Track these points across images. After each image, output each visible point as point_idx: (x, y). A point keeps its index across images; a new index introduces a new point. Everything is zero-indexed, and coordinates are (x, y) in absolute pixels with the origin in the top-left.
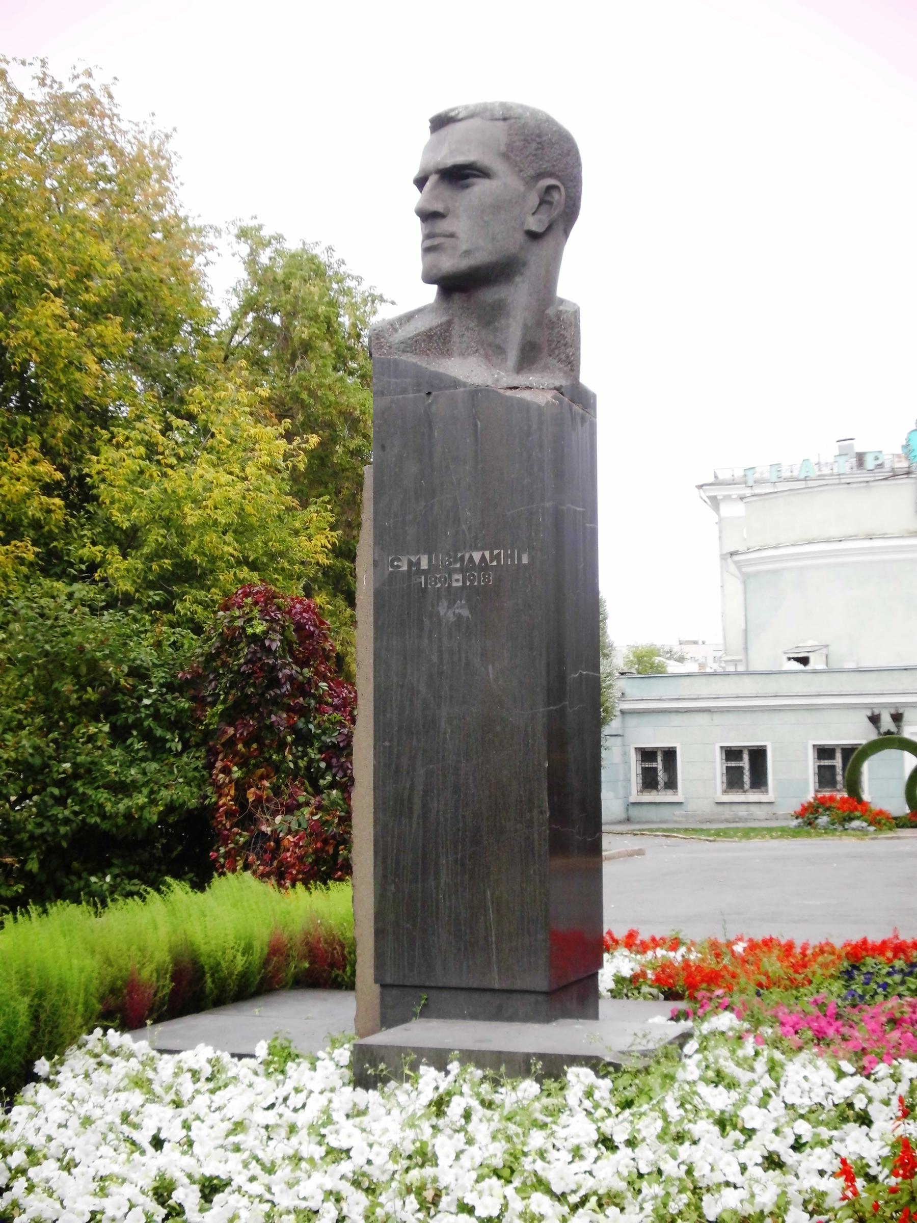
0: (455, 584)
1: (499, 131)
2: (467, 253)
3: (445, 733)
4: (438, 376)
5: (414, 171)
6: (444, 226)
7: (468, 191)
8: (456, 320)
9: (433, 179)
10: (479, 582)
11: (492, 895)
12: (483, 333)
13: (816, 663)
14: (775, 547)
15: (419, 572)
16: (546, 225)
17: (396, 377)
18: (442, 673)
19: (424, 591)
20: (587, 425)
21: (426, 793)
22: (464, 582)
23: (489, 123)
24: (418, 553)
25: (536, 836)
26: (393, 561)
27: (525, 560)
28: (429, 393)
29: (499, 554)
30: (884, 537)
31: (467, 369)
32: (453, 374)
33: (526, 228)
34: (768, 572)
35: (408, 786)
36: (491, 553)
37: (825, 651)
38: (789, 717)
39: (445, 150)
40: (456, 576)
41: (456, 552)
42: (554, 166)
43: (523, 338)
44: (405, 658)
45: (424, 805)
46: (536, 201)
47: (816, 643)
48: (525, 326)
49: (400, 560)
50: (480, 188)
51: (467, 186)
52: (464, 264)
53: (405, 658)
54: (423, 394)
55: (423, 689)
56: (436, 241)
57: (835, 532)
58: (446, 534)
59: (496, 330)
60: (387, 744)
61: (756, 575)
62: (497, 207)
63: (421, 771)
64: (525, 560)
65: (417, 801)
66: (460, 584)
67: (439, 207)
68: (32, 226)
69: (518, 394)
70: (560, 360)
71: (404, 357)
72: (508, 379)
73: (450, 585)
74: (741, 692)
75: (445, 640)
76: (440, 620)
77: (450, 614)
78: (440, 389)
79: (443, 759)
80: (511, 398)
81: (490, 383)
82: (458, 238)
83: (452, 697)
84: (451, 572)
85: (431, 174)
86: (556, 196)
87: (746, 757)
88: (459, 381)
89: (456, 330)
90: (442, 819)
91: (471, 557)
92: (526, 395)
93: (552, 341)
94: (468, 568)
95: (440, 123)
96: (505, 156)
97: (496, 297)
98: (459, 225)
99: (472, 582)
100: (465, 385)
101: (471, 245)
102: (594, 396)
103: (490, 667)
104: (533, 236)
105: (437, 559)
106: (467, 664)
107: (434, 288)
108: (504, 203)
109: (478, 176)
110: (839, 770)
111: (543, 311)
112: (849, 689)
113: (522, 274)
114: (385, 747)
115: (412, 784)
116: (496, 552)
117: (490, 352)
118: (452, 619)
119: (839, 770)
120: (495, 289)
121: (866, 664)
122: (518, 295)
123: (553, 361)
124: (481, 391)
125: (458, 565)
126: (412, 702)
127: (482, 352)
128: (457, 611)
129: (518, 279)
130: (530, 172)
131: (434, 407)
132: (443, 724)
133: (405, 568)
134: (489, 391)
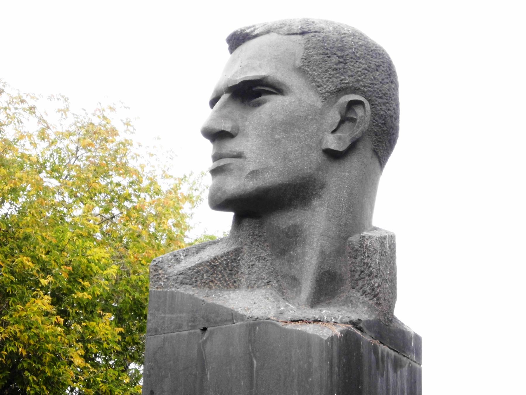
1: (297, 46)
2: (254, 173)
4: (216, 309)
5: (209, 95)
6: (231, 146)
9: (225, 97)
12: (277, 263)
16: (348, 143)
17: (172, 312)
20: (405, 371)
23: (285, 37)
28: (205, 329)
31: (249, 301)
32: (231, 307)
33: (324, 147)
39: (237, 67)
42: (358, 81)
43: (320, 266)
46: (338, 118)
48: (322, 252)
50: (273, 104)
51: (259, 104)
52: (251, 185)
54: (198, 331)
56: (222, 162)
62: (290, 124)
67: (227, 126)
68: (29, 230)
70: (364, 292)
71: (182, 290)
72: (293, 311)
78: (216, 323)
80: (290, 331)
81: (271, 316)
85: (222, 94)
86: (359, 112)
89: (245, 259)
92: (310, 329)
95: (237, 40)
96: (301, 71)
97: (291, 222)
98: (248, 144)
100: (242, 317)
101: (261, 162)
102: (418, 339)
104: (333, 155)
107: (229, 217)
108: (317, 133)
109: (271, 93)
111: (346, 239)
117: (285, 285)
122: (316, 222)
124: (259, 324)
127: (274, 284)
129: (315, 202)
130: (331, 87)
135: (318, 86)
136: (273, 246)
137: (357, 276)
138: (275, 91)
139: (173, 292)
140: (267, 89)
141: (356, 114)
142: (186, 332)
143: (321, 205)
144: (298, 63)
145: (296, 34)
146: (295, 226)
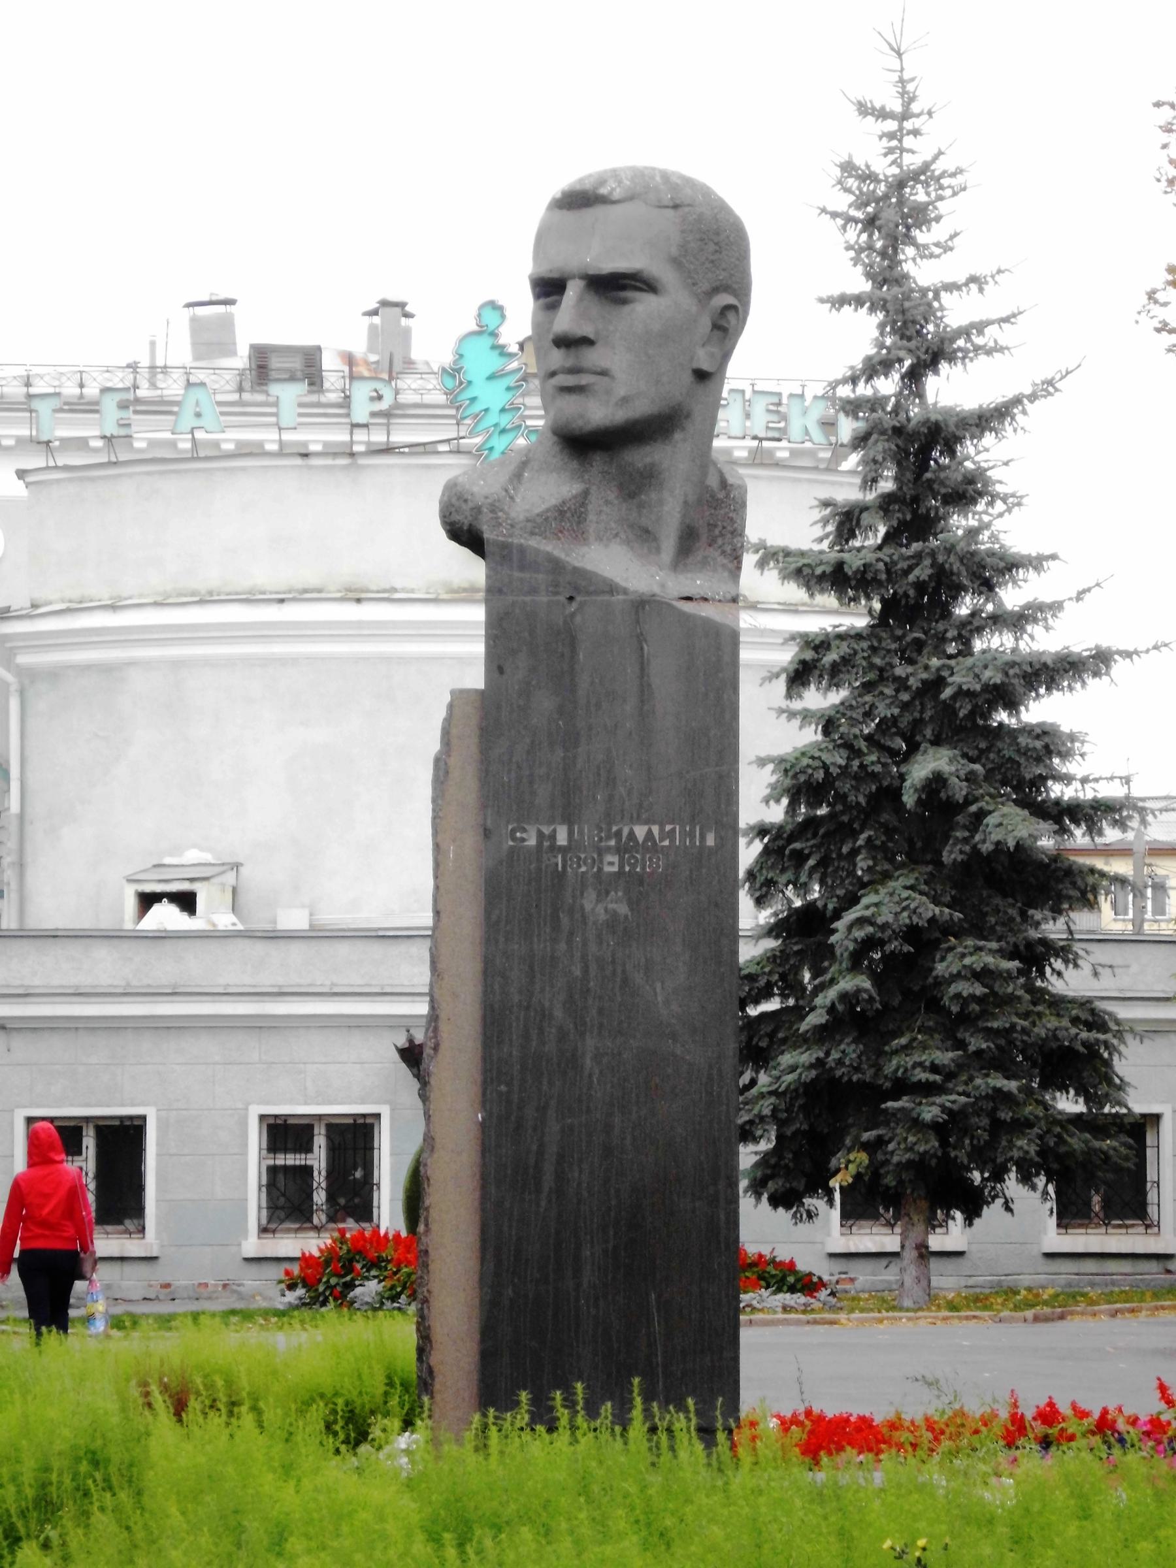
0: (608, 869)
2: (625, 400)
3: (590, 1076)
7: (626, 309)
8: (593, 490)
10: (643, 868)
11: (659, 1296)
13: (213, 912)
14: (113, 607)
15: (554, 848)
18: (588, 990)
19: (560, 876)
21: (561, 1157)
22: (621, 866)
24: (551, 821)
25: (722, 1217)
26: (513, 831)
27: (710, 841)
28: (571, 598)
29: (673, 830)
30: (388, 596)
33: (695, 365)
34: (86, 668)
35: (534, 1147)
36: (662, 830)
37: (230, 878)
38: (208, 1047)
40: (609, 858)
41: (610, 825)
44: (531, 968)
45: (560, 1176)
47: (208, 857)
49: (524, 830)
50: (644, 306)
51: (625, 302)
53: (531, 968)
54: (562, 598)
55: (558, 1013)
57: (263, 576)
58: (594, 798)
59: (641, 506)
60: (503, 1088)
61: (55, 674)
63: (553, 1128)
64: (710, 841)
65: (549, 1168)
66: (615, 869)
67: (587, 330)
69: (687, 607)
70: (723, 552)
73: (600, 869)
74: (83, 980)
75: (593, 948)
76: (584, 916)
77: (600, 909)
78: (589, 593)
79: (588, 1110)
82: (613, 378)
83: (601, 1025)
84: (601, 852)
85: (573, 277)
87: (320, 1140)
88: (617, 585)
90: (585, 1194)
91: (632, 834)
93: (716, 526)
94: (626, 848)
95: (578, 201)
96: (676, 262)
97: (648, 460)
99: (633, 866)
100: (625, 591)
103: (658, 985)
105: (581, 832)
106: (625, 981)
110: (320, 1178)
112: (352, 980)
113: (683, 429)
114: (500, 1094)
115: (541, 1145)
116: (668, 828)
118: (603, 917)
119: (320, 1178)
120: (648, 449)
121: (334, 916)
122: (671, 458)
123: (713, 553)
124: (648, 602)
125: (612, 843)
126: (541, 1030)
127: (623, 536)
128: (610, 906)
129: (678, 436)
130: (705, 286)
131: (578, 619)
132: (588, 1062)
133: (532, 842)
134: (660, 603)
135: (694, 284)
136: (621, 487)
137: (717, 532)
138: (645, 287)
139: (521, 545)
140: (638, 284)
141: (728, 322)
142: (545, 599)
143: (685, 440)
144: (674, 251)
145: (667, 207)
146: (652, 465)
